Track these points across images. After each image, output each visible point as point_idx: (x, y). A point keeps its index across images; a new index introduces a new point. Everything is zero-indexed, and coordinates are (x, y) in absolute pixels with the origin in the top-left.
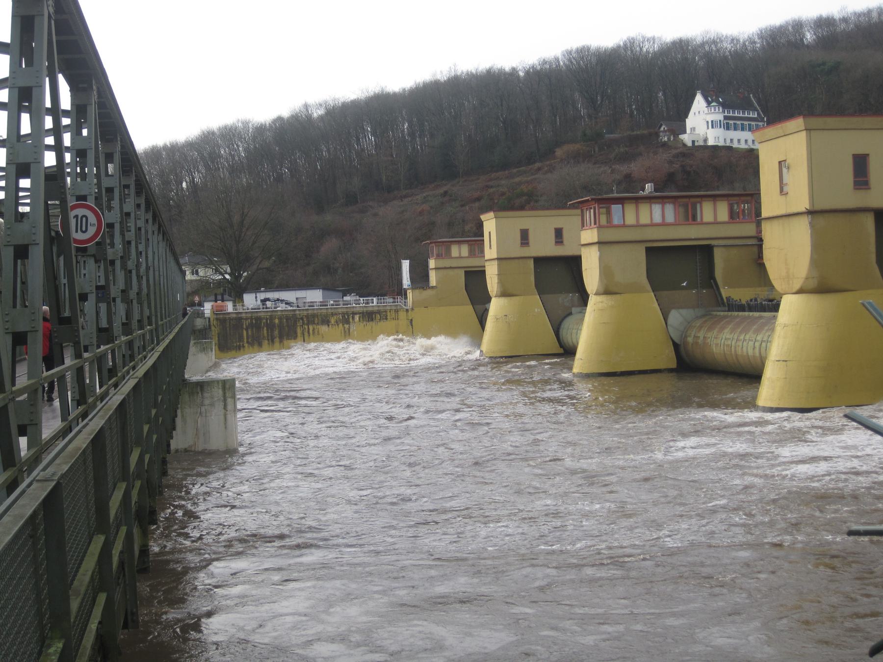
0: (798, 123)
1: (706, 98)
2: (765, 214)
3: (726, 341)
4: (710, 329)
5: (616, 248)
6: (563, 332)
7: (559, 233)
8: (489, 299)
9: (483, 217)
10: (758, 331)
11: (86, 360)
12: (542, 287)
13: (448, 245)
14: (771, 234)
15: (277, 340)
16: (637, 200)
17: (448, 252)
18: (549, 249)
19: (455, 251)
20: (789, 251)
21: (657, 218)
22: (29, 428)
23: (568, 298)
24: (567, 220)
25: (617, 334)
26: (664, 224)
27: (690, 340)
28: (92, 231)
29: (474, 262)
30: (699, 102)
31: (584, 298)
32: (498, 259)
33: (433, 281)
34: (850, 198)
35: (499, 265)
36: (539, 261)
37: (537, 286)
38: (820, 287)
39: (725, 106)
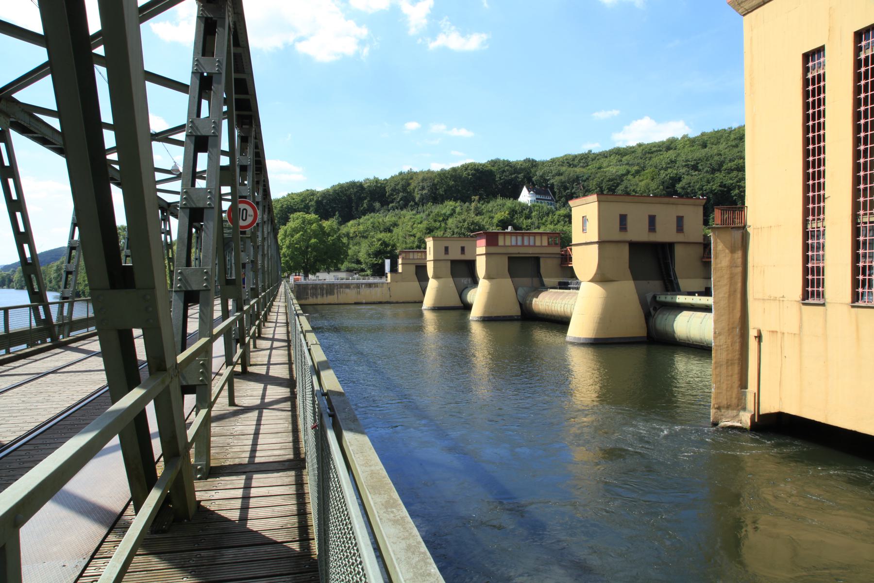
3: (547, 302)
6: (463, 296)
7: (463, 249)
11: (245, 312)
12: (454, 274)
18: (458, 256)
21: (514, 243)
22: (197, 388)
23: (466, 281)
25: (492, 298)
26: (517, 246)
28: (250, 220)
33: (400, 270)
34: (617, 235)
35: (599, 249)
38: (601, 278)
39: (537, 193)
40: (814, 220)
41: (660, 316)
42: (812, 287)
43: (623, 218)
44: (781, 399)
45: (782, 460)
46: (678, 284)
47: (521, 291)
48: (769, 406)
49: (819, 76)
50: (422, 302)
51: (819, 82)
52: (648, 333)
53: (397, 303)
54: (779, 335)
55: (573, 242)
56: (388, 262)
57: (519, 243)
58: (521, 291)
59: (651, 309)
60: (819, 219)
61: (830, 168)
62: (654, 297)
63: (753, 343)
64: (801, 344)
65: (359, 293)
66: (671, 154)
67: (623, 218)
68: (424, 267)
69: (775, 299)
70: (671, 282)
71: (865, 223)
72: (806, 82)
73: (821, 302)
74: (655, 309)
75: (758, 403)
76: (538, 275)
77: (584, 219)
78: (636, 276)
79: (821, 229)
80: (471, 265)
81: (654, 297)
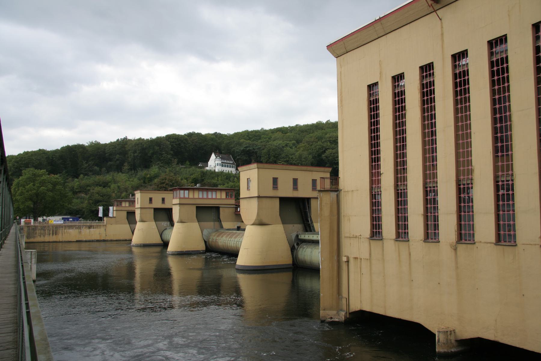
0: (254, 165)
1: (215, 155)
2: (241, 196)
4: (218, 236)
5: (186, 206)
6: (164, 236)
7: (163, 200)
8: (135, 223)
9: (135, 192)
10: (236, 237)
12: (156, 219)
13: (121, 202)
14: (243, 204)
15: (51, 235)
16: (194, 189)
17: (121, 204)
18: (159, 205)
19: (123, 204)
20: (249, 210)
23: (165, 224)
24: (167, 195)
26: (203, 198)
27: (210, 240)
29: (131, 209)
30: (213, 156)
31: (172, 225)
32: (140, 208)
34: (271, 192)
36: (156, 210)
37: (154, 218)
39: (222, 158)
40: (401, 185)
41: (301, 249)
42: (376, 230)
43: (275, 181)
44: (361, 301)
45: (196, 298)
46: (313, 226)
47: (206, 232)
48: (355, 306)
49: (430, 82)
50: (131, 240)
51: (464, 76)
52: (293, 262)
53: (111, 241)
54: (359, 260)
55: (241, 197)
56: (101, 209)
57: (205, 196)
58: (206, 232)
59: (295, 244)
60: (404, 184)
61: (382, 155)
62: (297, 236)
63: (344, 267)
64: (371, 266)
65: (80, 233)
66: (319, 133)
67: (275, 181)
68: (133, 213)
69: (356, 237)
70: (309, 226)
71: (503, 181)
72: (455, 76)
73: (381, 238)
74: (298, 244)
75: (348, 305)
76: (219, 220)
77: (248, 180)
78: (284, 222)
79: (510, 182)
80: (168, 212)
81: (297, 236)
